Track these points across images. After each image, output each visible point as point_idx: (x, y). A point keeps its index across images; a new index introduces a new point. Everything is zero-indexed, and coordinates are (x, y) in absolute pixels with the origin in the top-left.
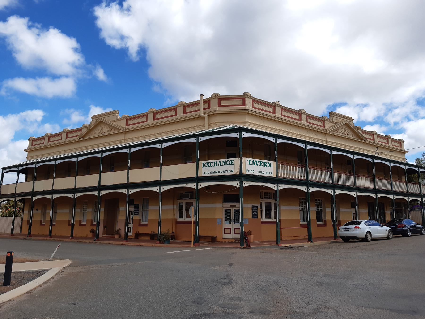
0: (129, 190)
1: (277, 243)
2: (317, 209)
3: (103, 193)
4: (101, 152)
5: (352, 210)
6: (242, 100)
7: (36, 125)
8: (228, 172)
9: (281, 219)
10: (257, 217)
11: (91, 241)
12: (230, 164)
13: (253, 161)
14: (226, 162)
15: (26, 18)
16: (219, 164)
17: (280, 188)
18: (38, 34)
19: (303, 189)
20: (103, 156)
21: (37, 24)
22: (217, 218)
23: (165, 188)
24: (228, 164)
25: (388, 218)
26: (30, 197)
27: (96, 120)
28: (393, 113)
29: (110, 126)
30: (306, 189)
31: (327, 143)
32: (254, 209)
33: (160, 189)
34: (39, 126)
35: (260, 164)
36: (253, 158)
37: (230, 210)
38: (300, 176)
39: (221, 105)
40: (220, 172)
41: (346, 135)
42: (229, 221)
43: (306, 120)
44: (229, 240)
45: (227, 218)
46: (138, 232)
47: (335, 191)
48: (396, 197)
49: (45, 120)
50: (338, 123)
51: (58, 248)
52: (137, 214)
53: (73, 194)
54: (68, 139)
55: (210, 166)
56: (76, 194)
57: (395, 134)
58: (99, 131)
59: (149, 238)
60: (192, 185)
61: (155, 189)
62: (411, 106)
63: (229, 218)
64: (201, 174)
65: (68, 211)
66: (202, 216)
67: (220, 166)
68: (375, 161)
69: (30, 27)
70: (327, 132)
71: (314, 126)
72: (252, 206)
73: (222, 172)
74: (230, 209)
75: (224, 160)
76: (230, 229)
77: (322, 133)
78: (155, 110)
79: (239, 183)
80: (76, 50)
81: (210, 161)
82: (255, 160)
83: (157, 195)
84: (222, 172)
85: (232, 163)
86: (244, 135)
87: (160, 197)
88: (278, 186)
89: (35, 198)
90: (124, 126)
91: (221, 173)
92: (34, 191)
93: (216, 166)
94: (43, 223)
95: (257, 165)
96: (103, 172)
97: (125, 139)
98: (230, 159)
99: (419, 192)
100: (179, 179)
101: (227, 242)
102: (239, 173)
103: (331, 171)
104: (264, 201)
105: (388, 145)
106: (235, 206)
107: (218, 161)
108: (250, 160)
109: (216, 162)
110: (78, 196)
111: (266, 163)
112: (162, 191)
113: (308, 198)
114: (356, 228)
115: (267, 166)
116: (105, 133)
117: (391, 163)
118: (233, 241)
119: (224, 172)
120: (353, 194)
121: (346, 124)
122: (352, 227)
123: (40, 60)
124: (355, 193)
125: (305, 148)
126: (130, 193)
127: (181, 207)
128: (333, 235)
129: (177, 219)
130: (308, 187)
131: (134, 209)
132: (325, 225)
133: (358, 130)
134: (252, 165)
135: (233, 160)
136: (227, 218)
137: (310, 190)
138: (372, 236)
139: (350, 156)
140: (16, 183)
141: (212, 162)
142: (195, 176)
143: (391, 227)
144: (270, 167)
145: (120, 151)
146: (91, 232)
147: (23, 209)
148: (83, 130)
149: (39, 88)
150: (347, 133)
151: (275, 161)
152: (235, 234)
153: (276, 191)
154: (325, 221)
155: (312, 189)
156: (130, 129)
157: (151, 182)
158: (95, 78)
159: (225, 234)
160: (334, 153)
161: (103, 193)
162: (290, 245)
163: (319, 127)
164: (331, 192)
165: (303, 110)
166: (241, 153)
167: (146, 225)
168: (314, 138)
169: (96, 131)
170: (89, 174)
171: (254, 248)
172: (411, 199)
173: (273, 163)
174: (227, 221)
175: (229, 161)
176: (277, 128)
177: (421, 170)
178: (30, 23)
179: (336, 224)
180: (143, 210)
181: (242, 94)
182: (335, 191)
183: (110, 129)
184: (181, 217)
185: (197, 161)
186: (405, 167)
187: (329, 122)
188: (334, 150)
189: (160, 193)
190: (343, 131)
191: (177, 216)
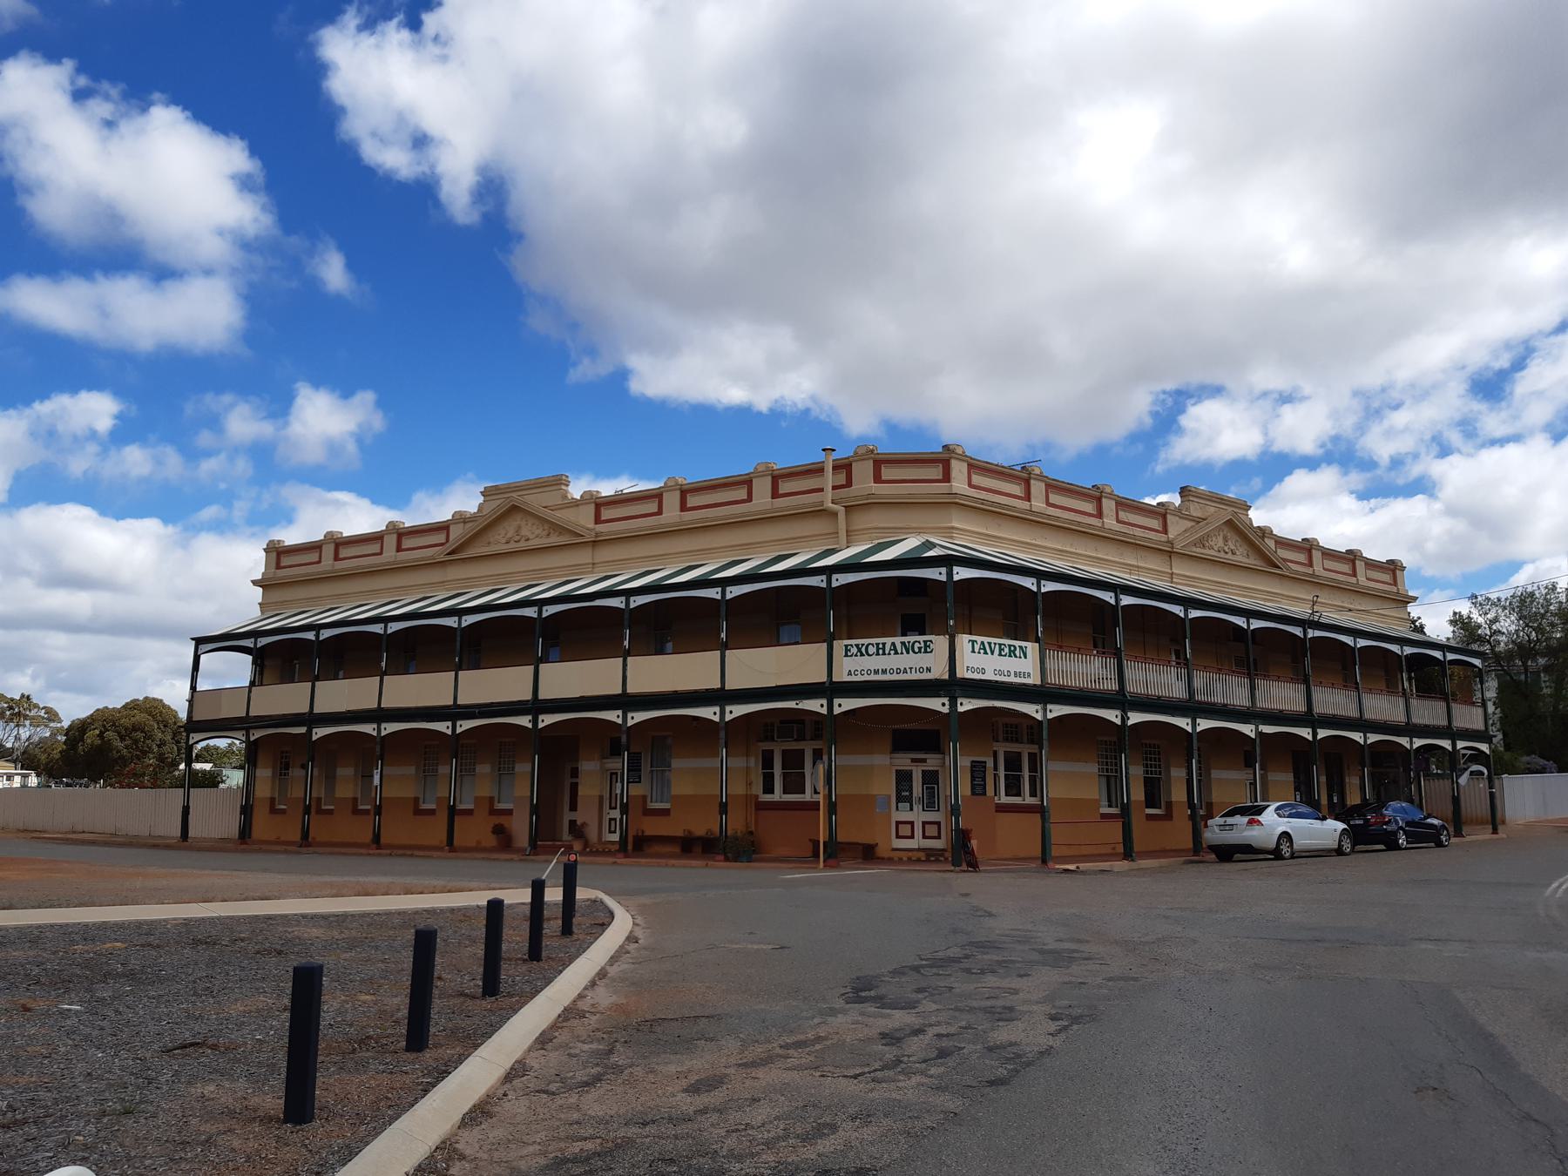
0: (630, 715)
1: (1044, 861)
2: (1147, 771)
3: (546, 720)
4: (539, 604)
5: (1242, 775)
6: (941, 465)
7: (92, 448)
10: (985, 794)
12: (923, 650)
13: (983, 643)
15: (64, 60)
16: (891, 650)
17: (1050, 716)
18: (109, 118)
19: (1113, 715)
20: (545, 615)
21: (105, 86)
23: (737, 711)
24: (917, 650)
25: (1353, 799)
26: (303, 730)
28: (1386, 423)
29: (543, 520)
30: (1120, 717)
31: (1174, 580)
32: (977, 770)
33: (723, 713)
34: (104, 453)
35: (1001, 650)
36: (973, 632)
38: (1099, 679)
41: (1229, 556)
43: (1115, 516)
44: (910, 854)
46: (643, 832)
47: (1198, 721)
48: (1373, 738)
49: (123, 434)
50: (1204, 519)
52: (636, 782)
53: (449, 724)
54: (403, 556)
57: (1396, 497)
58: (509, 535)
59: (677, 850)
60: (816, 705)
61: (709, 713)
62: (1452, 401)
63: (908, 794)
64: (841, 676)
65: (411, 770)
66: (842, 788)
68: (1311, 633)
69: (79, 96)
70: (1173, 548)
71: (1138, 532)
72: (973, 762)
76: (912, 823)
77: (1160, 550)
78: (685, 482)
79: (947, 703)
80: (245, 184)
81: (866, 641)
82: (986, 640)
85: (926, 648)
86: (958, 573)
87: (722, 734)
88: (1045, 710)
89: (319, 733)
90: (591, 525)
92: (315, 712)
94: (361, 807)
95: (992, 653)
97: (595, 562)
99: (1445, 723)
100: (777, 687)
101: (905, 859)
102: (946, 677)
103: (1185, 664)
104: (1002, 748)
105: (1353, 580)
106: (924, 760)
107: (888, 641)
108: (973, 642)
109: (884, 644)
110: (463, 729)
111: (1014, 646)
112: (728, 717)
113: (1124, 738)
114: (1251, 822)
115: (1018, 655)
116: (530, 543)
117: (1358, 640)
118: (922, 856)
120: (1248, 729)
121: (1230, 523)
122: (1242, 820)
123: (111, 215)
124: (1253, 727)
125: (1114, 604)
126: (630, 723)
127: (768, 762)
128: (1191, 846)
129: (757, 796)
130: (1124, 712)
132: (1168, 816)
133: (1263, 537)
134: (979, 653)
135: (931, 641)
136: (903, 795)
137: (1128, 718)
138: (1295, 846)
139: (1240, 621)
140: (248, 685)
141: (873, 645)
142: (825, 680)
143: (1352, 823)
144: (1025, 657)
145: (598, 603)
146: (493, 832)
149: (104, 312)
150: (1233, 548)
151: (1036, 642)
152: (924, 837)
153: (1040, 723)
154: (1169, 805)
155: (1135, 718)
156: (610, 533)
157: (696, 692)
158: (313, 286)
160: (1194, 614)
161: (546, 720)
162: (1078, 868)
163: (1152, 535)
164: (1188, 724)
165: (1105, 487)
166: (952, 623)
167: (666, 812)
168: (1138, 567)
169: (499, 534)
170: (477, 667)
171: (985, 871)
172: (1418, 743)
173: (1032, 648)
174: (902, 802)
175: (919, 642)
176: (1034, 542)
177: (1450, 657)
178: (82, 81)
179: (1200, 814)
180: (500, 774)
181: (941, 450)
182: (1198, 721)
183: (544, 530)
184: (769, 789)
185: (830, 640)
186: (1402, 648)
187: (1180, 518)
188: (1196, 606)
189: (723, 724)
190: (1220, 543)
191: (757, 789)
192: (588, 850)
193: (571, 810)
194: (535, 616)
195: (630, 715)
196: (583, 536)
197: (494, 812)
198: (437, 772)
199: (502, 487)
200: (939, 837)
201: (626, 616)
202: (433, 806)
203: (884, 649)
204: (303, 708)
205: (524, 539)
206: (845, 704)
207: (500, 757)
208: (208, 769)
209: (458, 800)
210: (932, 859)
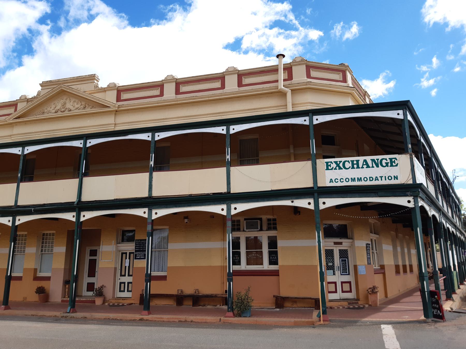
6: (341, 73)
8: (386, 180)
9: (356, 265)
11: (58, 314)
12: (389, 164)
14: (379, 161)
16: (363, 165)
23: (242, 207)
24: (384, 165)
33: (229, 209)
37: (347, 251)
42: (332, 269)
45: (329, 265)
53: (11, 218)
55: (342, 167)
56: (17, 218)
58: (58, 108)
67: (366, 168)
73: (373, 179)
74: (332, 250)
75: (375, 157)
76: (335, 283)
81: (343, 159)
83: (187, 222)
85: (392, 163)
91: (370, 180)
98: (388, 157)
100: (272, 191)
106: (341, 243)
109: (358, 161)
131: (136, 248)
135: (396, 159)
141: (348, 161)
146: (36, 292)
148: (20, 106)
152: (343, 292)
157: (208, 195)
161: (87, 215)
167: (164, 278)
169: (51, 108)
175: (386, 159)
180: (42, 254)
183: (81, 105)
184: (237, 262)
192: (106, 304)
193: (89, 276)
195: (154, 211)
197: (36, 278)
199: (53, 81)
200: (350, 291)
201: (152, 145)
203: (358, 164)
205: (67, 110)
207: (42, 247)
208: (400, 248)
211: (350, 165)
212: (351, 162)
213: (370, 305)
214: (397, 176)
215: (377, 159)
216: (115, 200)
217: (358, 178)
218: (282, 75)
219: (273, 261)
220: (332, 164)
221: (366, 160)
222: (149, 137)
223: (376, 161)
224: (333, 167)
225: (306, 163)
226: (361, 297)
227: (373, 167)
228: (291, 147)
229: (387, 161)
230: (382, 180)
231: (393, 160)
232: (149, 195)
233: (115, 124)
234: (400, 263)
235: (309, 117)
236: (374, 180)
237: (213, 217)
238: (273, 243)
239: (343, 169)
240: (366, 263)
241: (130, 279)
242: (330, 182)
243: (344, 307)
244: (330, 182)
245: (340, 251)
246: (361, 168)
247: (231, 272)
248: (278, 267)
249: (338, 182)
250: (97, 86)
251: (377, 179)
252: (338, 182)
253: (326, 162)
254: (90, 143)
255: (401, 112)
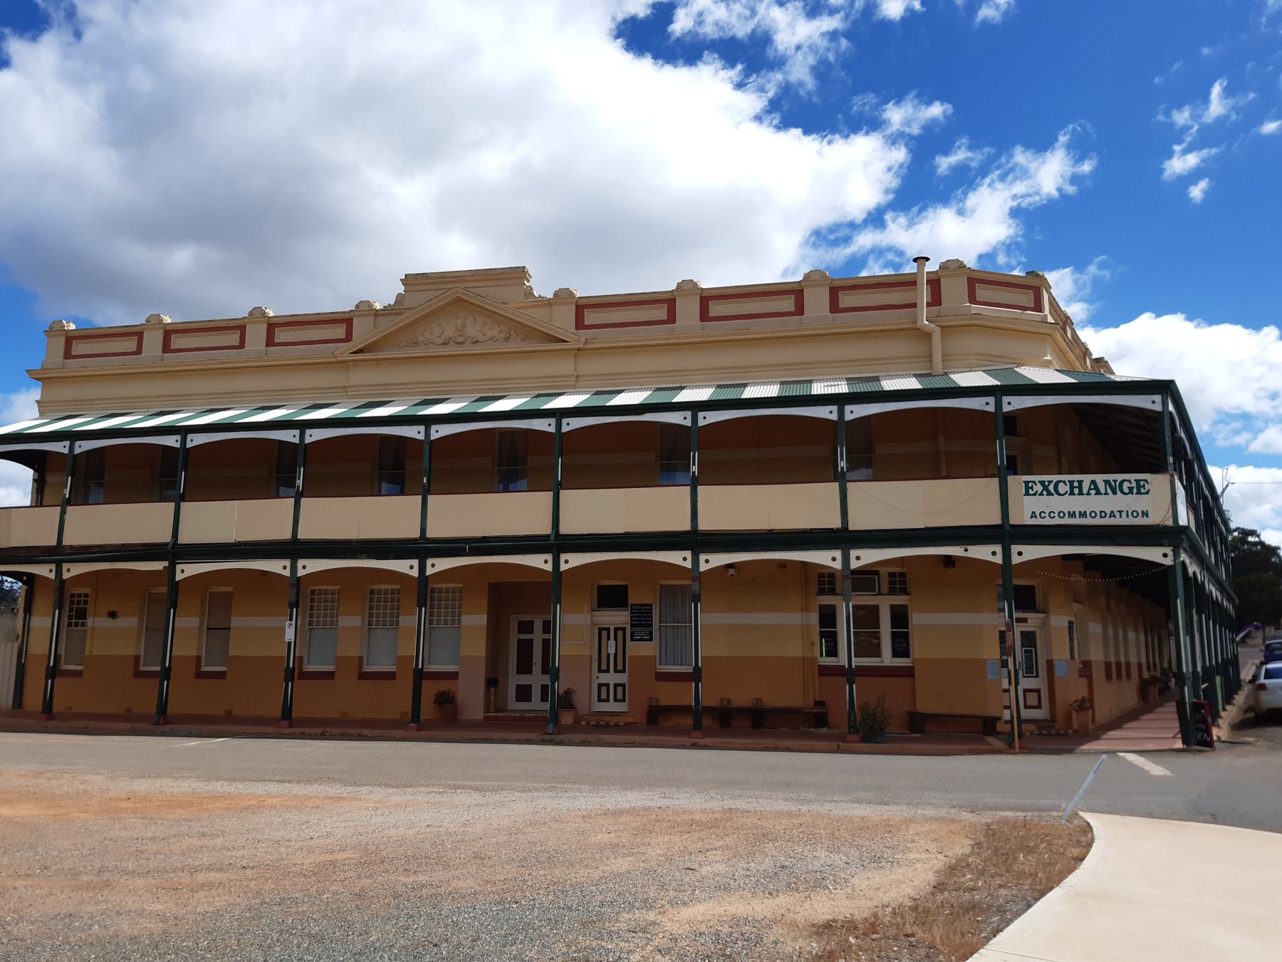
4: (183, 432)
8: (1128, 517)
12: (1135, 491)
14: (1118, 483)
16: (1090, 489)
22: (985, 658)
24: (1126, 490)
27: (442, 292)
39: (841, 305)
40: (1098, 514)
46: (657, 700)
51: (1094, 773)
55: (1053, 492)
56: (429, 562)
67: (1095, 494)
75: (1110, 477)
81: (1055, 478)
83: (732, 575)
84: (1064, 516)
85: (1139, 489)
89: (187, 570)
91: (1101, 517)
93: (1078, 494)
96: (186, 499)
100: (927, 529)
106: (1024, 620)
107: (1087, 479)
109: (1080, 482)
119: (1115, 517)
127: (828, 617)
131: (631, 621)
135: (1146, 481)
141: (1064, 482)
147: (28, 610)
159: (598, 701)
169: (432, 333)
175: (1130, 481)
180: (311, 629)
183: (501, 331)
184: (833, 652)
194: (178, 445)
196: (565, 341)
198: (337, 625)
200: (1039, 706)
202: (329, 668)
203: (1080, 487)
204: (164, 536)
206: (865, 557)
209: (426, 663)
210: (1045, 732)
211: (1067, 488)
212: (1068, 484)
213: (1075, 731)
214: (1147, 511)
215: (1113, 481)
216: (626, 533)
217: (1080, 512)
218: (924, 294)
219: (901, 649)
220: (1036, 485)
221: (1095, 481)
222: (685, 418)
223: (1113, 483)
224: (1037, 491)
225: (990, 481)
226: (1059, 716)
227: (1106, 493)
228: (941, 439)
229: (1131, 483)
230: (1121, 517)
231: (1142, 483)
232: (692, 528)
233: (577, 376)
234: (1113, 659)
235: (995, 397)
236: (1108, 516)
237: (785, 567)
238: (900, 617)
239: (1055, 494)
240: (1069, 657)
241: (622, 678)
242: (1031, 518)
243: (1032, 733)
244: (1031, 518)
245: (1023, 634)
246: (1087, 494)
247: (853, 667)
248: (911, 661)
249: (1045, 517)
250: (529, 292)
251: (1112, 515)
252: (1045, 517)
253: (1024, 482)
254: (568, 424)
255: (1158, 398)
